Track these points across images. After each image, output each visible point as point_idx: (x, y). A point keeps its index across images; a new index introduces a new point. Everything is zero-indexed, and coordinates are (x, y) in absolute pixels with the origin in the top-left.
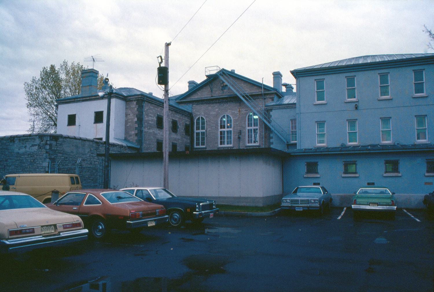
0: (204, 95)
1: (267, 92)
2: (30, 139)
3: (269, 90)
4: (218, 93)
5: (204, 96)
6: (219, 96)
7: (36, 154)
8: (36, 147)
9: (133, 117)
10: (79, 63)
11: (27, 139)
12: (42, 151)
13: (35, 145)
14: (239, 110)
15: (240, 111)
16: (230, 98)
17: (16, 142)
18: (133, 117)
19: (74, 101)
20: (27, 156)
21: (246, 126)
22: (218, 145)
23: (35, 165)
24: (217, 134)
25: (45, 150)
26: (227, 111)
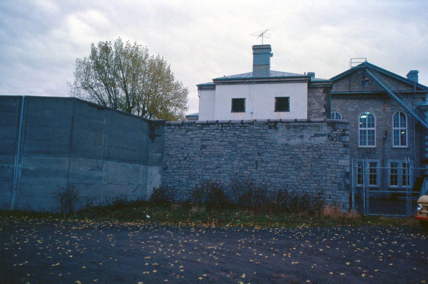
0: (340, 89)
1: (418, 91)
2: (310, 126)
3: (421, 89)
4: (356, 89)
5: (339, 91)
6: (358, 91)
7: (325, 147)
8: (325, 138)
9: (319, 107)
10: (136, 42)
11: (303, 126)
12: (334, 144)
13: (322, 135)
14: (383, 108)
15: (384, 109)
16: (373, 94)
17: (281, 129)
18: (319, 107)
19: (244, 82)
20: (306, 150)
21: (392, 126)
22: (358, 146)
23: (322, 162)
24: (357, 134)
25: (342, 143)
26: (369, 109)
